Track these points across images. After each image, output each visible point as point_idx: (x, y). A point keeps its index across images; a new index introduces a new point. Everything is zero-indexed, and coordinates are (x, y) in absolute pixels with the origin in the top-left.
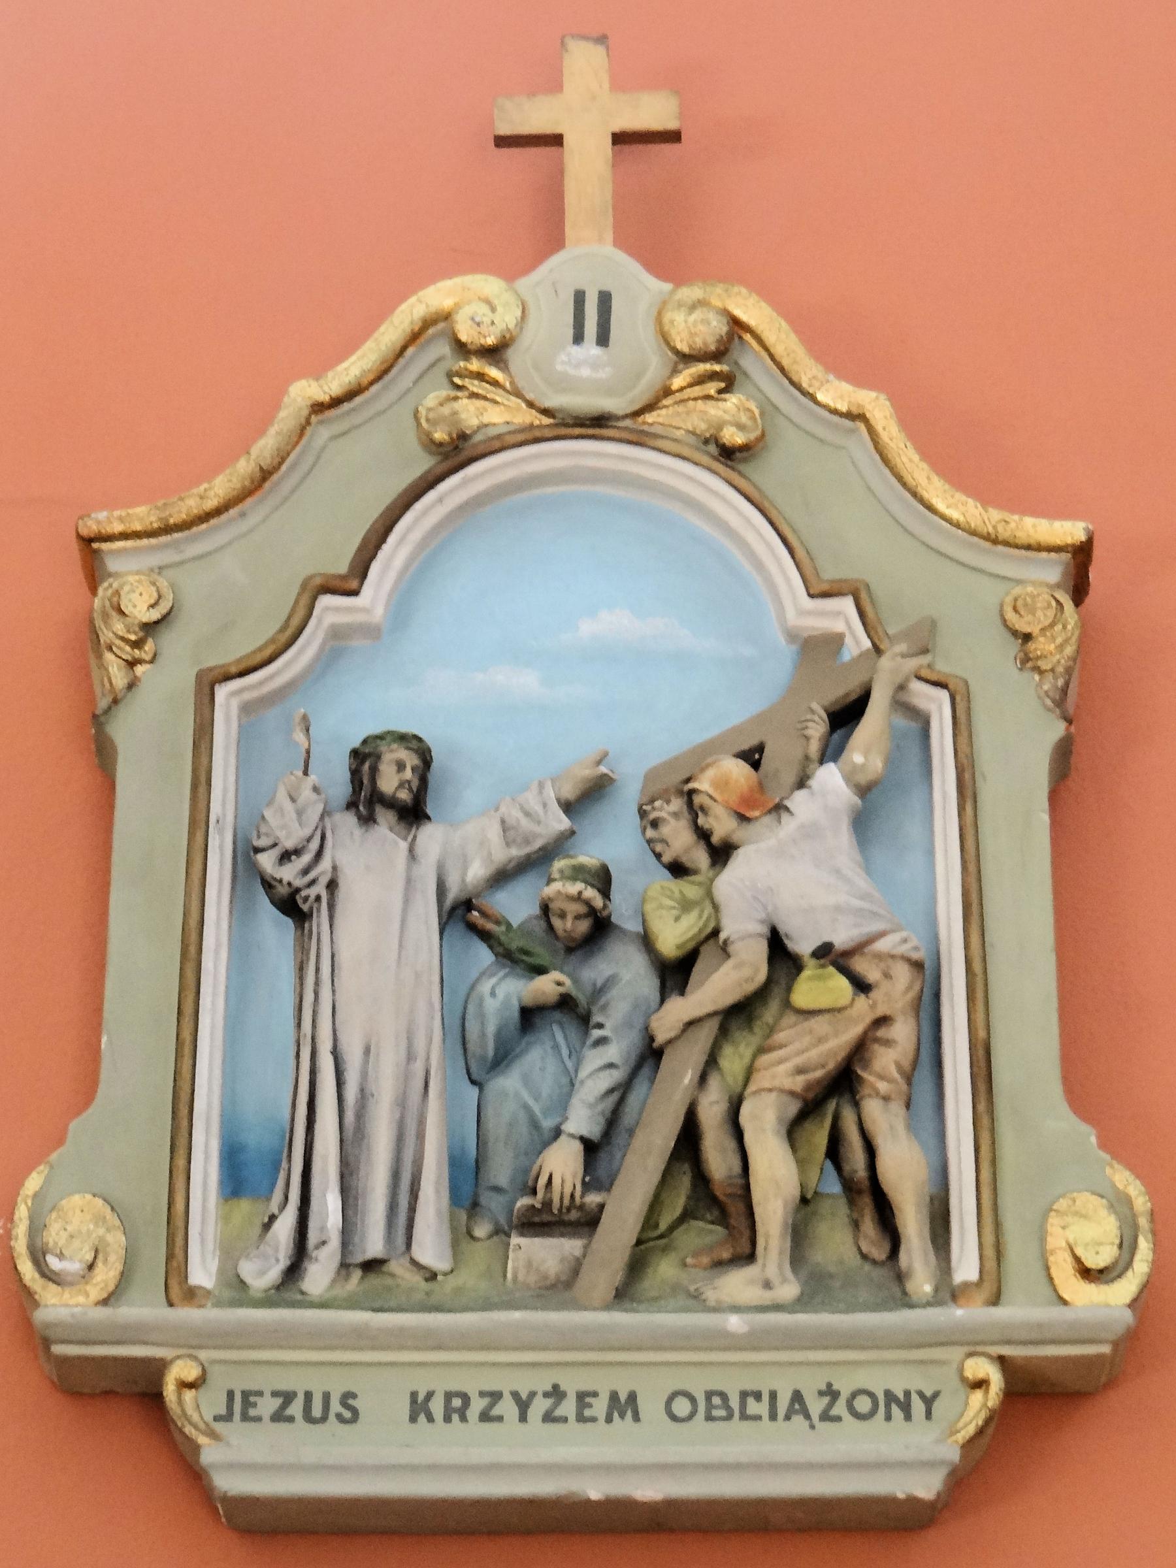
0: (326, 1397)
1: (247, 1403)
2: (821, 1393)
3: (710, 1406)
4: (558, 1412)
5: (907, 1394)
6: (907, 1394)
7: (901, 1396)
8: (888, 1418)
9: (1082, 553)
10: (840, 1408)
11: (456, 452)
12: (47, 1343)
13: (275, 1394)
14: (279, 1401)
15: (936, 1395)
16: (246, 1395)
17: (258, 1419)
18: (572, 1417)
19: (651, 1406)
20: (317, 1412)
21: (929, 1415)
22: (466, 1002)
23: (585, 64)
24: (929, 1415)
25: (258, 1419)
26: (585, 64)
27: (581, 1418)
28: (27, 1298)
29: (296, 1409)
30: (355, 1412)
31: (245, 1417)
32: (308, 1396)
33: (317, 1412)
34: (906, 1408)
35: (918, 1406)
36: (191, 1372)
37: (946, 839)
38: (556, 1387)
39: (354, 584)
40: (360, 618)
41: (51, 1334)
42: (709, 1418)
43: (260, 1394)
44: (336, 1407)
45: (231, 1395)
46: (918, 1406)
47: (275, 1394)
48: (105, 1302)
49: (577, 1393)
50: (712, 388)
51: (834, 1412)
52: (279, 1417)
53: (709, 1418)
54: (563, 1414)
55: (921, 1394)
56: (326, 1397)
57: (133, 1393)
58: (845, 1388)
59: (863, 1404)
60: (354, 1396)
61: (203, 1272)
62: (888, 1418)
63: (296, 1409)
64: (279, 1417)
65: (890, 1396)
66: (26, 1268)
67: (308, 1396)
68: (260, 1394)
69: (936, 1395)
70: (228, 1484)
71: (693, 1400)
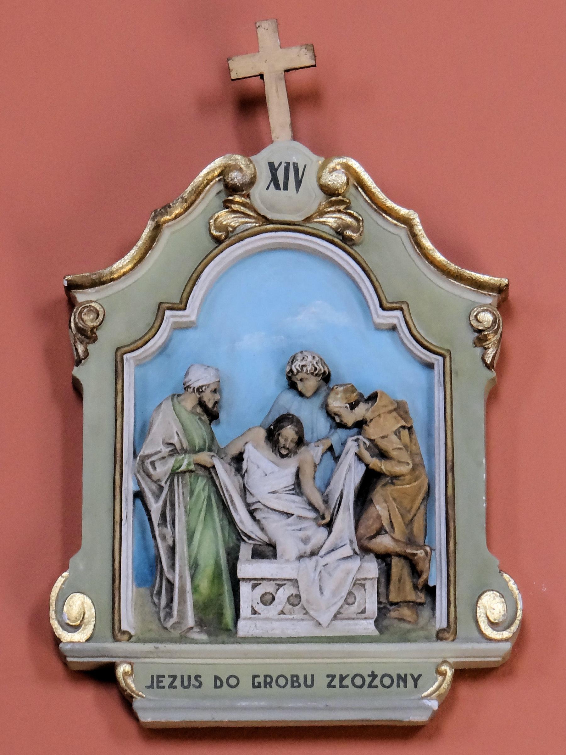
0: (189, 677)
1: (159, 682)
2: (369, 676)
3: (293, 682)
4: (333, 684)
5: (406, 675)
6: (406, 675)
7: (403, 676)
8: (398, 686)
9: (501, 290)
10: (377, 682)
11: (221, 240)
12: (65, 657)
13: (169, 676)
14: (171, 679)
15: (420, 676)
16: (158, 677)
17: (164, 687)
18: (338, 685)
19: (246, 682)
20: (186, 683)
21: (416, 686)
22: (390, 518)
23: (267, 34)
24: (416, 686)
25: (164, 687)
26: (267, 34)
27: (341, 686)
28: (57, 641)
29: (178, 683)
30: (201, 684)
31: (158, 687)
32: (182, 677)
33: (186, 683)
34: (405, 680)
35: (410, 682)
36: (128, 668)
37: (127, 563)
38: (373, 672)
39: (182, 306)
40: (184, 320)
41: (66, 654)
42: (292, 686)
43: (164, 676)
44: (193, 681)
45: (152, 677)
46: (410, 682)
47: (169, 676)
48: (87, 641)
49: (157, 676)
50: (342, 208)
51: (374, 684)
52: (171, 686)
53: (292, 686)
54: (347, 684)
55: (412, 676)
56: (189, 677)
57: (103, 675)
58: (379, 674)
59: (387, 681)
60: (200, 676)
61: (128, 620)
62: (398, 686)
63: (178, 683)
64: (171, 686)
65: (399, 676)
66: (55, 624)
67: (182, 677)
68: (164, 676)
69: (420, 676)
70: (146, 717)
71: (286, 678)
